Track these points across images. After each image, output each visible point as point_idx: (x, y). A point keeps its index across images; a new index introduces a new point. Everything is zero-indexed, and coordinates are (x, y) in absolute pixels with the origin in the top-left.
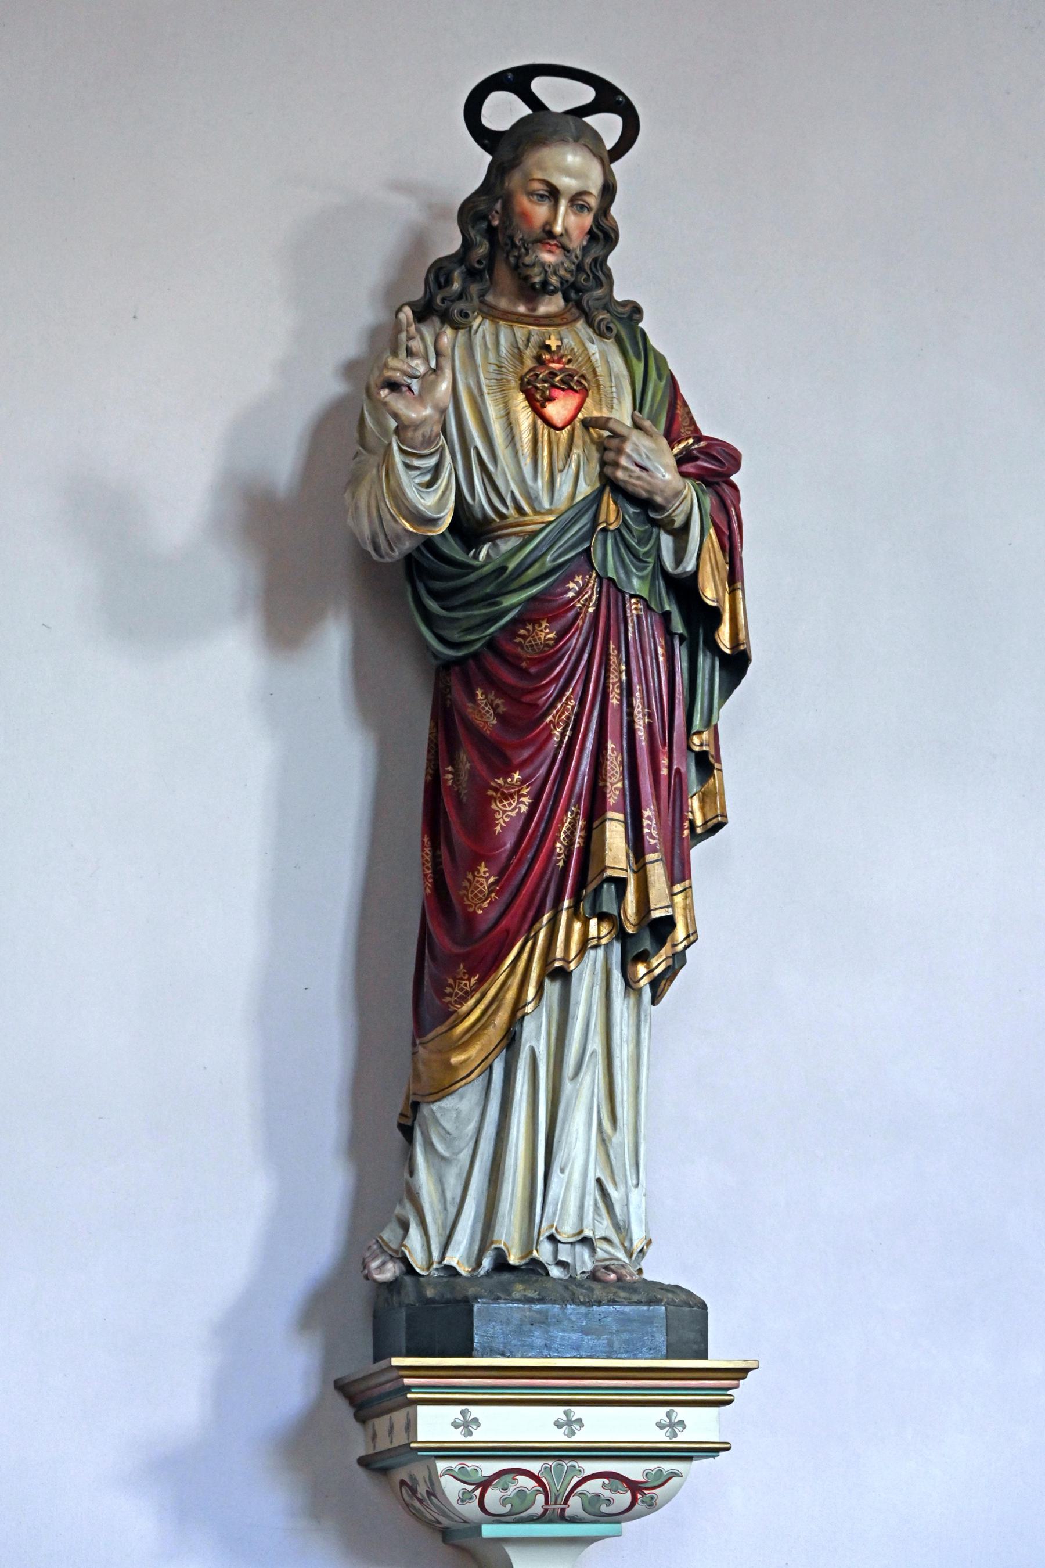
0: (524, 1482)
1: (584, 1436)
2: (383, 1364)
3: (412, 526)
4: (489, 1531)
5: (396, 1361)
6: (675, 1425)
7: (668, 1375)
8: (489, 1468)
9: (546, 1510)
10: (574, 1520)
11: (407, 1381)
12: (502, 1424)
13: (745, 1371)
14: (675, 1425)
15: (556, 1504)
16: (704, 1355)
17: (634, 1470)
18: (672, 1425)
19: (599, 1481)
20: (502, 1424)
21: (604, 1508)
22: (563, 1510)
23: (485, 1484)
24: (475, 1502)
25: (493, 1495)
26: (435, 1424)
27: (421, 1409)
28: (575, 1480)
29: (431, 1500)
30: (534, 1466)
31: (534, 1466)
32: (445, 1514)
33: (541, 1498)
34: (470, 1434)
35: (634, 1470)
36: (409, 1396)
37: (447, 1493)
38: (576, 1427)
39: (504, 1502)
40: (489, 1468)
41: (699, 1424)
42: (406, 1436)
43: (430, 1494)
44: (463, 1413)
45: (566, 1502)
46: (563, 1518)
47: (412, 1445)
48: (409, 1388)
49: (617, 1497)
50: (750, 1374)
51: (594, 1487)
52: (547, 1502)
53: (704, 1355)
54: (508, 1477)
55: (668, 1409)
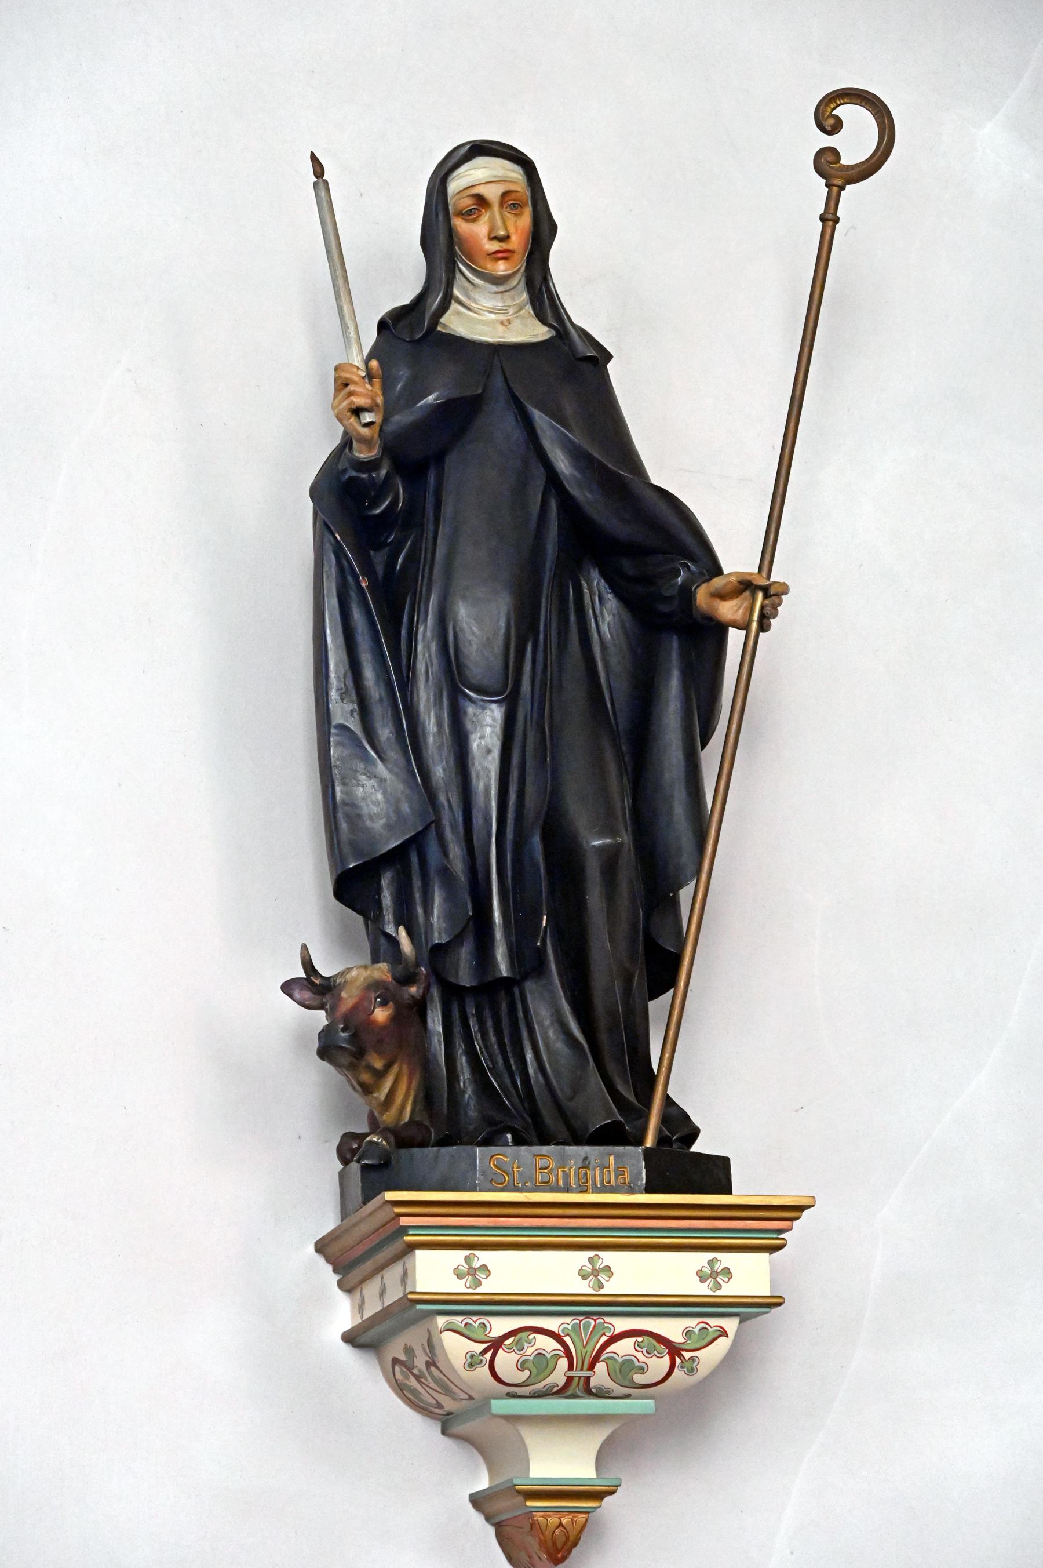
0: (548, 1345)
1: (612, 1287)
2: (376, 1202)
3: (385, 500)
4: (500, 1406)
5: (390, 1196)
6: (473, 1273)
7: (761, 1214)
8: (499, 1326)
9: (570, 1379)
10: (601, 1394)
11: (404, 1221)
12: (512, 1272)
13: (801, 1208)
14: (473, 1273)
15: (582, 1370)
16: (729, 1192)
17: (673, 1329)
18: (595, 1272)
19: (631, 1341)
20: (512, 1272)
21: (638, 1378)
22: (588, 1379)
23: (496, 1345)
24: (486, 1368)
25: (506, 1361)
26: (435, 1272)
27: (419, 1253)
28: (604, 1339)
29: (430, 1373)
30: (552, 1324)
31: (552, 1324)
32: (447, 1391)
33: (563, 1363)
34: (720, 1287)
35: (673, 1329)
36: (407, 1239)
37: (451, 1357)
38: (481, 1275)
39: (522, 1366)
40: (499, 1326)
41: (748, 1274)
42: (401, 1289)
43: (431, 1364)
44: (591, 1260)
45: (591, 1368)
46: (589, 1392)
47: (410, 1296)
48: (404, 1230)
49: (652, 1362)
50: (805, 1213)
51: (624, 1348)
52: (570, 1367)
53: (729, 1192)
54: (524, 1335)
55: (591, 1253)
